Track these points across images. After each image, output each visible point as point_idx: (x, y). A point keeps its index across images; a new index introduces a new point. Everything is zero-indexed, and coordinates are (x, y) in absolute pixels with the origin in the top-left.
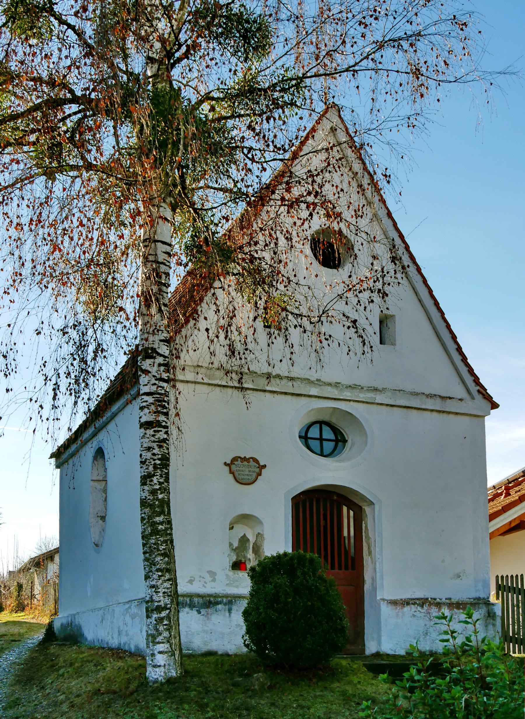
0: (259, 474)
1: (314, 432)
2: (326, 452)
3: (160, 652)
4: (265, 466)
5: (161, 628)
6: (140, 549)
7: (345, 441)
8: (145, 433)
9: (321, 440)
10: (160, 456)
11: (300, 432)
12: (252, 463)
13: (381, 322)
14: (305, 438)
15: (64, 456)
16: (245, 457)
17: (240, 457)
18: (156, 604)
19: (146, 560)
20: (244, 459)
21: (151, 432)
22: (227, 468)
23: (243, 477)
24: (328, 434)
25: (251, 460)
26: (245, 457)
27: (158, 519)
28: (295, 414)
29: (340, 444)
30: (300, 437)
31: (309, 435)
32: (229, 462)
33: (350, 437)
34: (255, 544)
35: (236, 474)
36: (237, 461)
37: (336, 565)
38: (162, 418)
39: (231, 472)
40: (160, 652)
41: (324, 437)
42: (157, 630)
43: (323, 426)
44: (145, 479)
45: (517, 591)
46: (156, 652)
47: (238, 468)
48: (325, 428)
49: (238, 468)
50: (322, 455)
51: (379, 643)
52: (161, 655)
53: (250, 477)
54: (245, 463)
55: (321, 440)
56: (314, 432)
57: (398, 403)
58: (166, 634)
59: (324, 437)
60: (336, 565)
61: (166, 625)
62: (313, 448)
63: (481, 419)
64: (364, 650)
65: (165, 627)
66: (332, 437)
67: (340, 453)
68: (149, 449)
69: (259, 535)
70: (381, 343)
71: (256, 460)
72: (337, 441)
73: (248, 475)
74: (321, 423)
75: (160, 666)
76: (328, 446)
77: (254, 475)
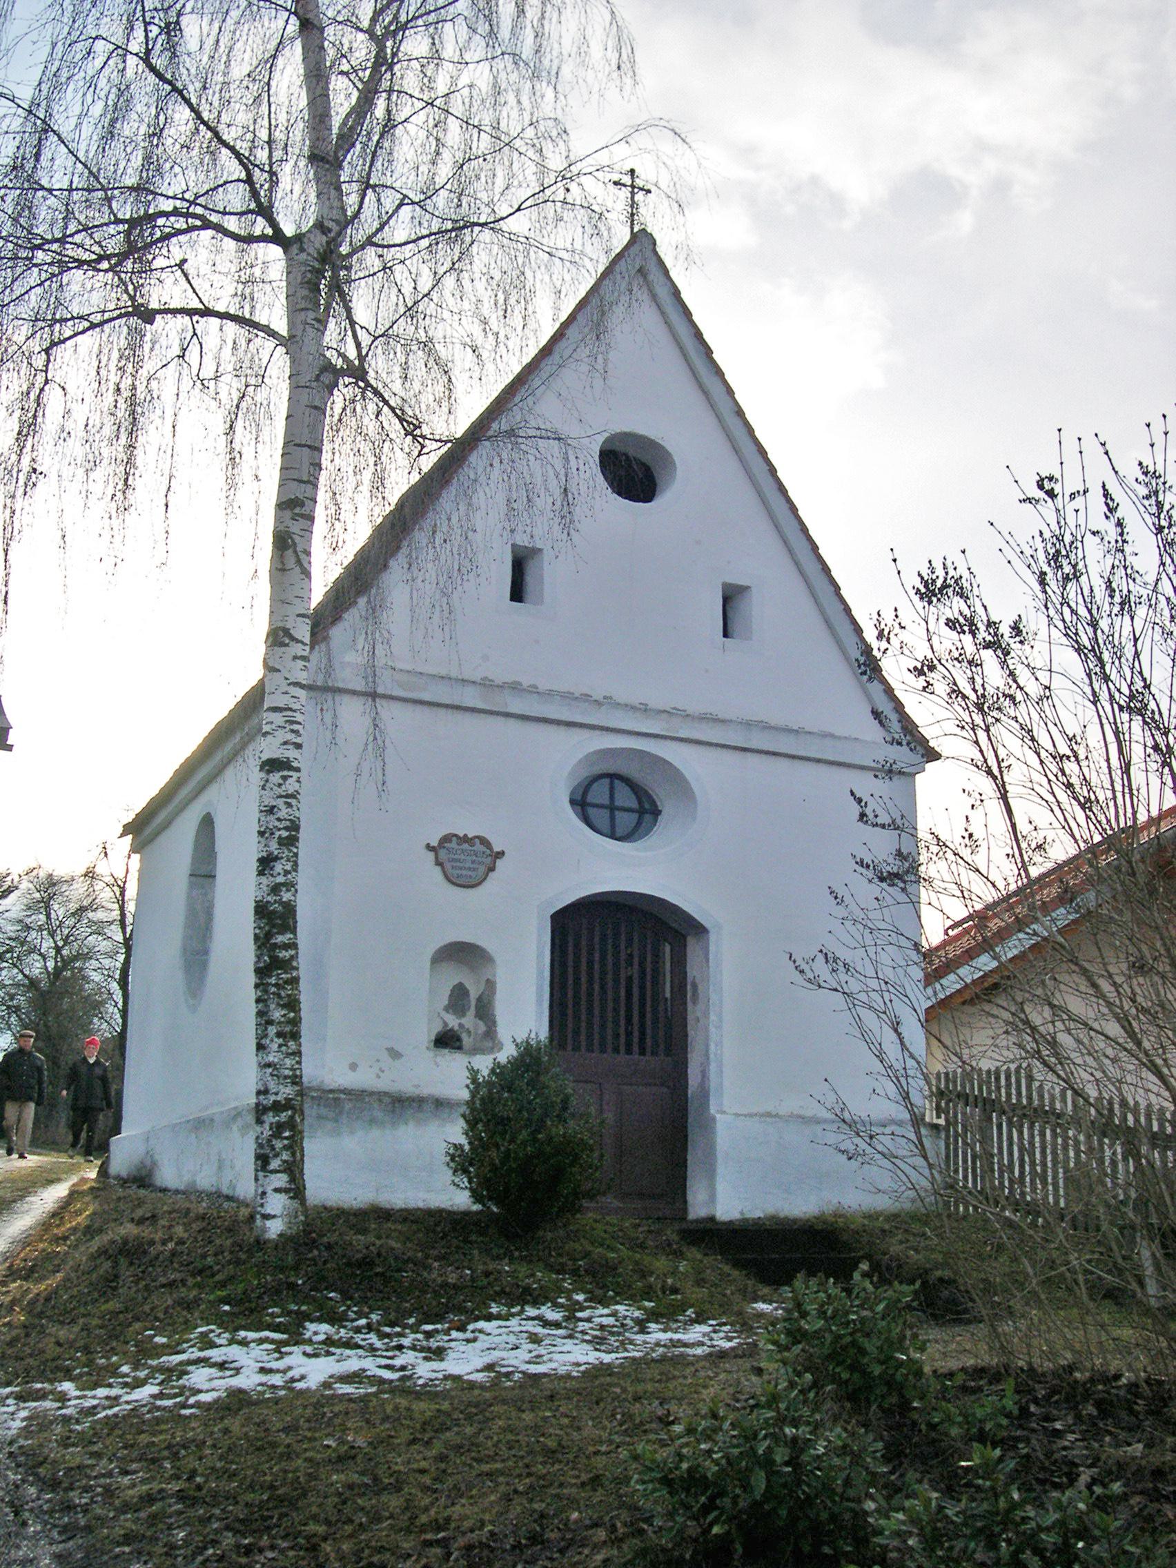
0: (492, 869)
1: (599, 794)
2: (619, 832)
3: (277, 1190)
4: (503, 853)
5: (278, 1144)
6: (252, 994)
7: (656, 813)
8: (267, 781)
9: (612, 808)
10: (288, 823)
11: (572, 793)
12: (479, 847)
13: (726, 600)
14: (581, 803)
15: (148, 831)
16: (465, 835)
17: (456, 835)
18: (273, 1098)
19: (260, 1014)
20: (465, 839)
21: (276, 778)
22: (431, 855)
23: (459, 872)
24: (625, 797)
25: (477, 841)
26: (465, 835)
27: (280, 939)
28: (564, 757)
29: (647, 817)
30: (573, 802)
31: (590, 799)
32: (434, 843)
33: (668, 808)
34: (479, 1000)
35: (448, 866)
36: (450, 841)
37: (636, 1048)
38: (291, 753)
39: (438, 863)
40: (277, 1190)
41: (618, 803)
42: (273, 1148)
43: (616, 782)
44: (266, 863)
45: (971, 1099)
46: (269, 1190)
47: (451, 856)
48: (621, 788)
49: (451, 856)
50: (613, 836)
51: (712, 1198)
52: (278, 1196)
53: (473, 874)
54: (466, 846)
55: (612, 808)
56: (599, 794)
57: (753, 744)
58: (285, 1156)
59: (618, 803)
60: (636, 1048)
61: (286, 1138)
62: (599, 826)
63: (909, 779)
64: (685, 1210)
65: (286, 1142)
66: (634, 804)
67: (648, 831)
68: (271, 810)
69: (490, 985)
70: (726, 635)
71: (484, 841)
72: (641, 812)
73: (470, 869)
74: (612, 777)
75: (274, 1217)
76: (625, 821)
77: (482, 869)
